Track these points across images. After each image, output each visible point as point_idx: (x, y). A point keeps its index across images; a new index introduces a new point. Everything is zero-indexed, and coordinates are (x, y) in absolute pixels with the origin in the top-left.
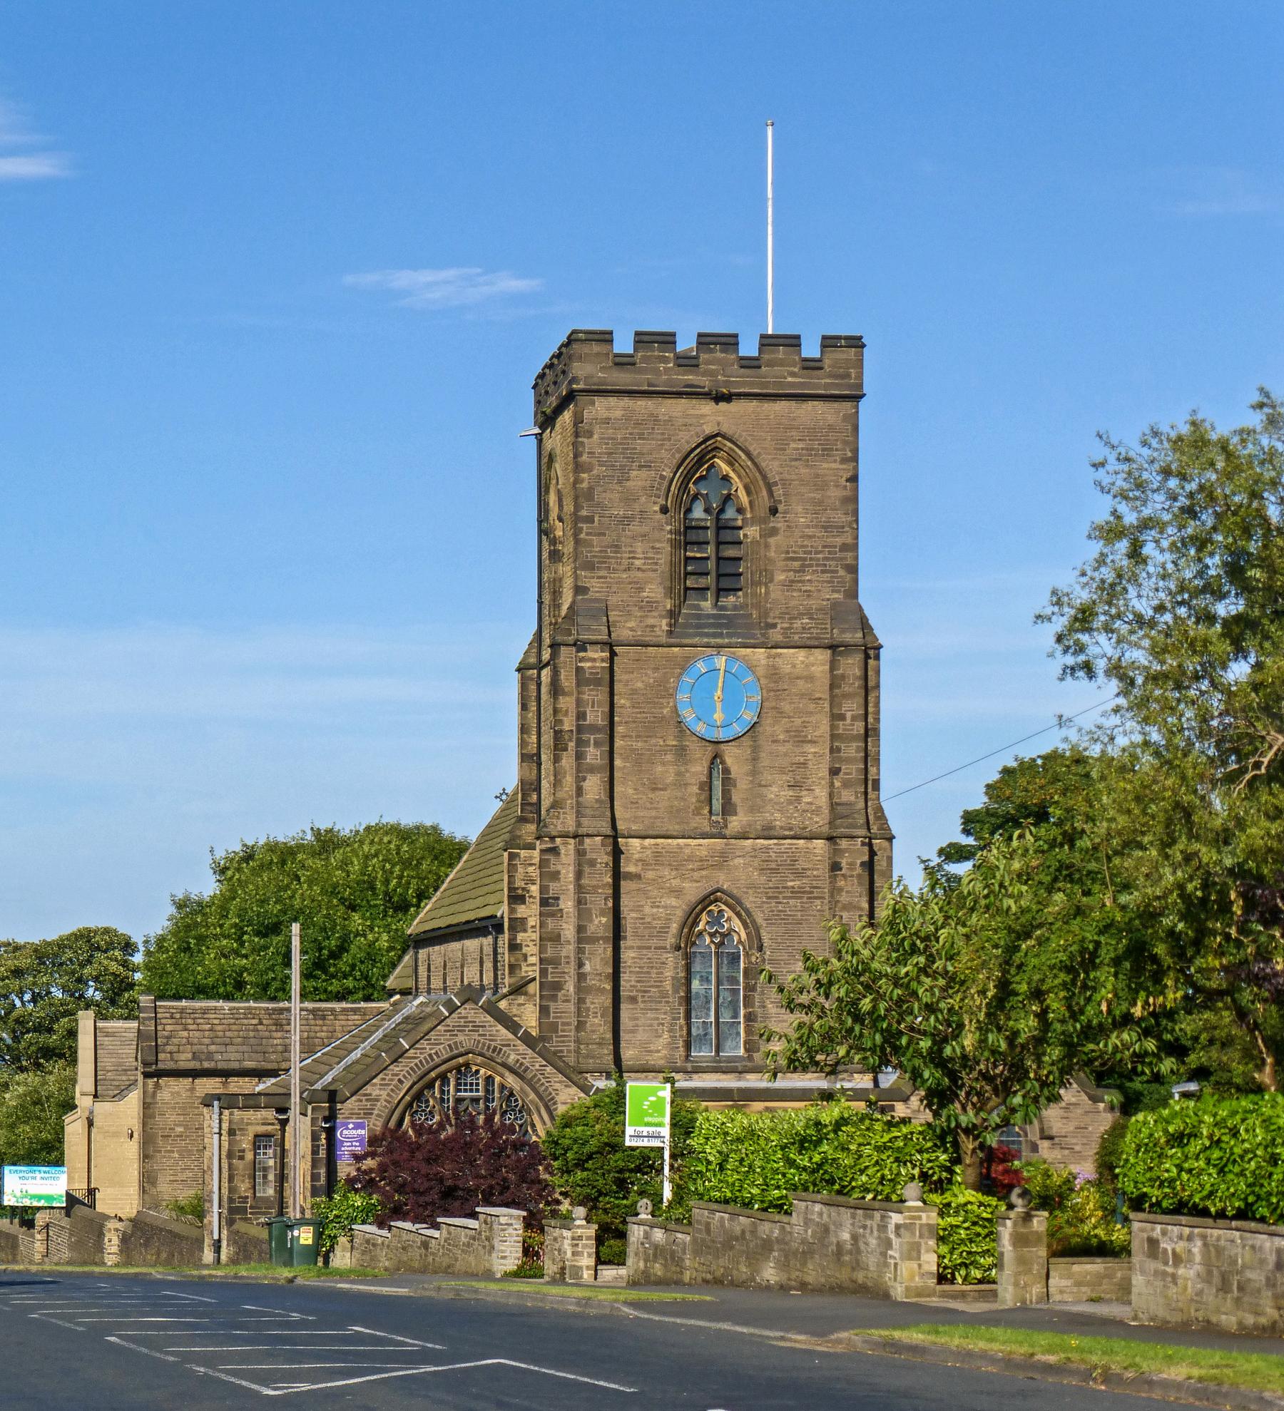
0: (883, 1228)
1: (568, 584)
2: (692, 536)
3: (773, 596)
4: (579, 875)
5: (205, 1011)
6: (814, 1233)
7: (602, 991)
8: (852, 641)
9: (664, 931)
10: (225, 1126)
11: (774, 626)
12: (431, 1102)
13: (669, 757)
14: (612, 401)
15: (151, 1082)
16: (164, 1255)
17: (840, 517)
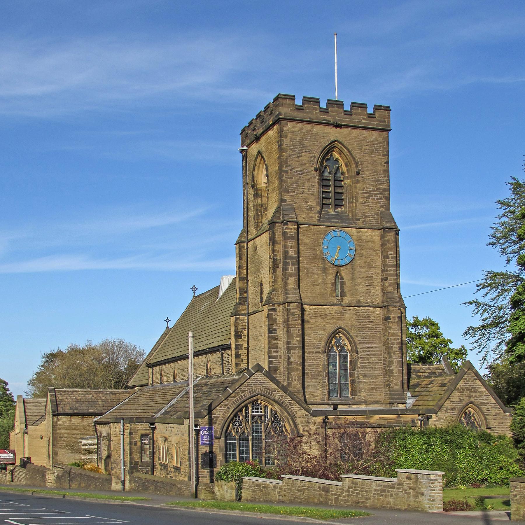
2: (325, 183)
3: (358, 207)
5: (73, 392)
7: (298, 369)
8: (391, 226)
9: (319, 344)
11: (359, 220)
12: (241, 418)
13: (320, 272)
14: (295, 124)
15: (55, 418)
16: (83, 485)
17: (382, 178)
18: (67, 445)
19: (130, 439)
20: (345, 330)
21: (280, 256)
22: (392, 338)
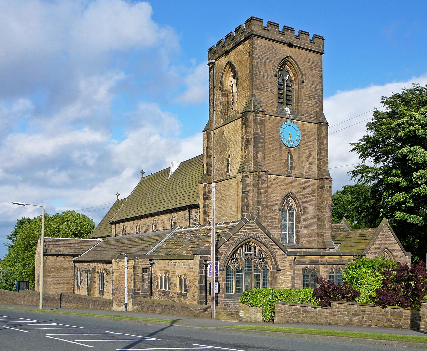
9: (276, 204)
14: (262, 40)
17: (318, 87)
18: (53, 277)
19: (134, 271)
21: (251, 136)
22: (326, 201)
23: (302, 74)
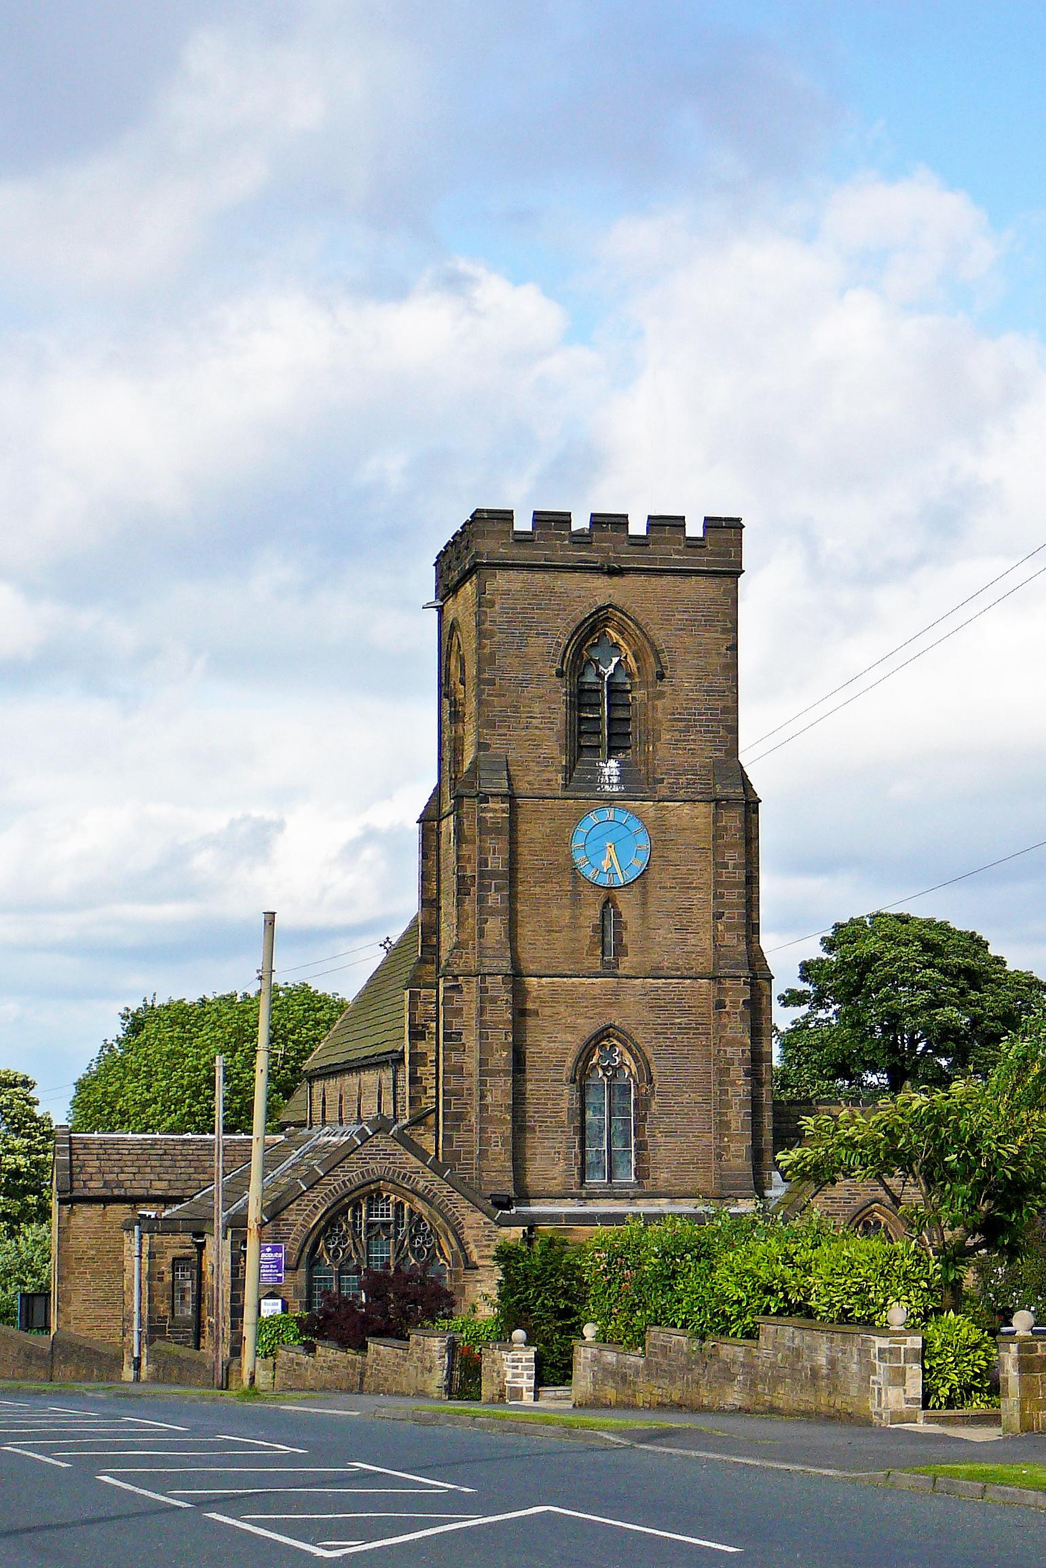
0: (864, 1352)
1: (470, 740)
4: (481, 1011)
6: (785, 1358)
7: (502, 1121)
8: (733, 796)
10: (146, 1249)
14: (512, 574)
15: (66, 1208)
17: (721, 682)
20: (623, 1032)
22: (729, 1049)
23: (657, 654)
